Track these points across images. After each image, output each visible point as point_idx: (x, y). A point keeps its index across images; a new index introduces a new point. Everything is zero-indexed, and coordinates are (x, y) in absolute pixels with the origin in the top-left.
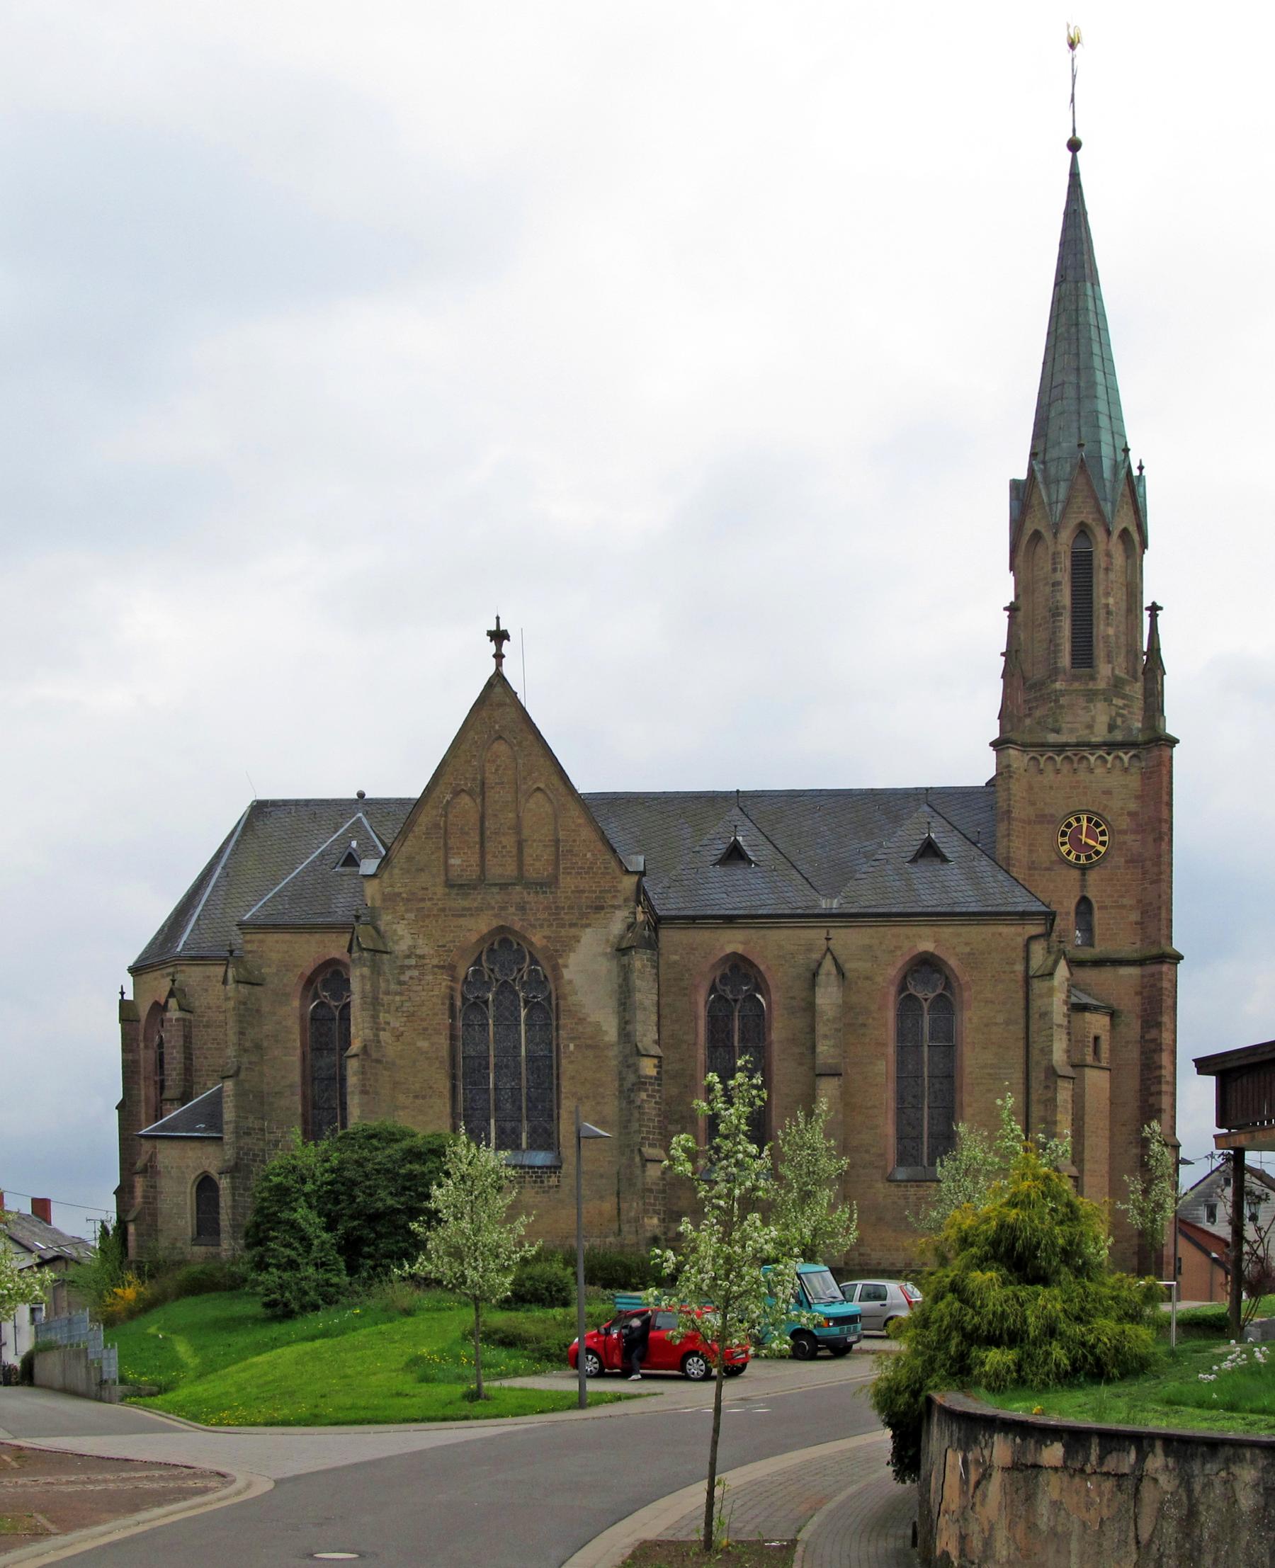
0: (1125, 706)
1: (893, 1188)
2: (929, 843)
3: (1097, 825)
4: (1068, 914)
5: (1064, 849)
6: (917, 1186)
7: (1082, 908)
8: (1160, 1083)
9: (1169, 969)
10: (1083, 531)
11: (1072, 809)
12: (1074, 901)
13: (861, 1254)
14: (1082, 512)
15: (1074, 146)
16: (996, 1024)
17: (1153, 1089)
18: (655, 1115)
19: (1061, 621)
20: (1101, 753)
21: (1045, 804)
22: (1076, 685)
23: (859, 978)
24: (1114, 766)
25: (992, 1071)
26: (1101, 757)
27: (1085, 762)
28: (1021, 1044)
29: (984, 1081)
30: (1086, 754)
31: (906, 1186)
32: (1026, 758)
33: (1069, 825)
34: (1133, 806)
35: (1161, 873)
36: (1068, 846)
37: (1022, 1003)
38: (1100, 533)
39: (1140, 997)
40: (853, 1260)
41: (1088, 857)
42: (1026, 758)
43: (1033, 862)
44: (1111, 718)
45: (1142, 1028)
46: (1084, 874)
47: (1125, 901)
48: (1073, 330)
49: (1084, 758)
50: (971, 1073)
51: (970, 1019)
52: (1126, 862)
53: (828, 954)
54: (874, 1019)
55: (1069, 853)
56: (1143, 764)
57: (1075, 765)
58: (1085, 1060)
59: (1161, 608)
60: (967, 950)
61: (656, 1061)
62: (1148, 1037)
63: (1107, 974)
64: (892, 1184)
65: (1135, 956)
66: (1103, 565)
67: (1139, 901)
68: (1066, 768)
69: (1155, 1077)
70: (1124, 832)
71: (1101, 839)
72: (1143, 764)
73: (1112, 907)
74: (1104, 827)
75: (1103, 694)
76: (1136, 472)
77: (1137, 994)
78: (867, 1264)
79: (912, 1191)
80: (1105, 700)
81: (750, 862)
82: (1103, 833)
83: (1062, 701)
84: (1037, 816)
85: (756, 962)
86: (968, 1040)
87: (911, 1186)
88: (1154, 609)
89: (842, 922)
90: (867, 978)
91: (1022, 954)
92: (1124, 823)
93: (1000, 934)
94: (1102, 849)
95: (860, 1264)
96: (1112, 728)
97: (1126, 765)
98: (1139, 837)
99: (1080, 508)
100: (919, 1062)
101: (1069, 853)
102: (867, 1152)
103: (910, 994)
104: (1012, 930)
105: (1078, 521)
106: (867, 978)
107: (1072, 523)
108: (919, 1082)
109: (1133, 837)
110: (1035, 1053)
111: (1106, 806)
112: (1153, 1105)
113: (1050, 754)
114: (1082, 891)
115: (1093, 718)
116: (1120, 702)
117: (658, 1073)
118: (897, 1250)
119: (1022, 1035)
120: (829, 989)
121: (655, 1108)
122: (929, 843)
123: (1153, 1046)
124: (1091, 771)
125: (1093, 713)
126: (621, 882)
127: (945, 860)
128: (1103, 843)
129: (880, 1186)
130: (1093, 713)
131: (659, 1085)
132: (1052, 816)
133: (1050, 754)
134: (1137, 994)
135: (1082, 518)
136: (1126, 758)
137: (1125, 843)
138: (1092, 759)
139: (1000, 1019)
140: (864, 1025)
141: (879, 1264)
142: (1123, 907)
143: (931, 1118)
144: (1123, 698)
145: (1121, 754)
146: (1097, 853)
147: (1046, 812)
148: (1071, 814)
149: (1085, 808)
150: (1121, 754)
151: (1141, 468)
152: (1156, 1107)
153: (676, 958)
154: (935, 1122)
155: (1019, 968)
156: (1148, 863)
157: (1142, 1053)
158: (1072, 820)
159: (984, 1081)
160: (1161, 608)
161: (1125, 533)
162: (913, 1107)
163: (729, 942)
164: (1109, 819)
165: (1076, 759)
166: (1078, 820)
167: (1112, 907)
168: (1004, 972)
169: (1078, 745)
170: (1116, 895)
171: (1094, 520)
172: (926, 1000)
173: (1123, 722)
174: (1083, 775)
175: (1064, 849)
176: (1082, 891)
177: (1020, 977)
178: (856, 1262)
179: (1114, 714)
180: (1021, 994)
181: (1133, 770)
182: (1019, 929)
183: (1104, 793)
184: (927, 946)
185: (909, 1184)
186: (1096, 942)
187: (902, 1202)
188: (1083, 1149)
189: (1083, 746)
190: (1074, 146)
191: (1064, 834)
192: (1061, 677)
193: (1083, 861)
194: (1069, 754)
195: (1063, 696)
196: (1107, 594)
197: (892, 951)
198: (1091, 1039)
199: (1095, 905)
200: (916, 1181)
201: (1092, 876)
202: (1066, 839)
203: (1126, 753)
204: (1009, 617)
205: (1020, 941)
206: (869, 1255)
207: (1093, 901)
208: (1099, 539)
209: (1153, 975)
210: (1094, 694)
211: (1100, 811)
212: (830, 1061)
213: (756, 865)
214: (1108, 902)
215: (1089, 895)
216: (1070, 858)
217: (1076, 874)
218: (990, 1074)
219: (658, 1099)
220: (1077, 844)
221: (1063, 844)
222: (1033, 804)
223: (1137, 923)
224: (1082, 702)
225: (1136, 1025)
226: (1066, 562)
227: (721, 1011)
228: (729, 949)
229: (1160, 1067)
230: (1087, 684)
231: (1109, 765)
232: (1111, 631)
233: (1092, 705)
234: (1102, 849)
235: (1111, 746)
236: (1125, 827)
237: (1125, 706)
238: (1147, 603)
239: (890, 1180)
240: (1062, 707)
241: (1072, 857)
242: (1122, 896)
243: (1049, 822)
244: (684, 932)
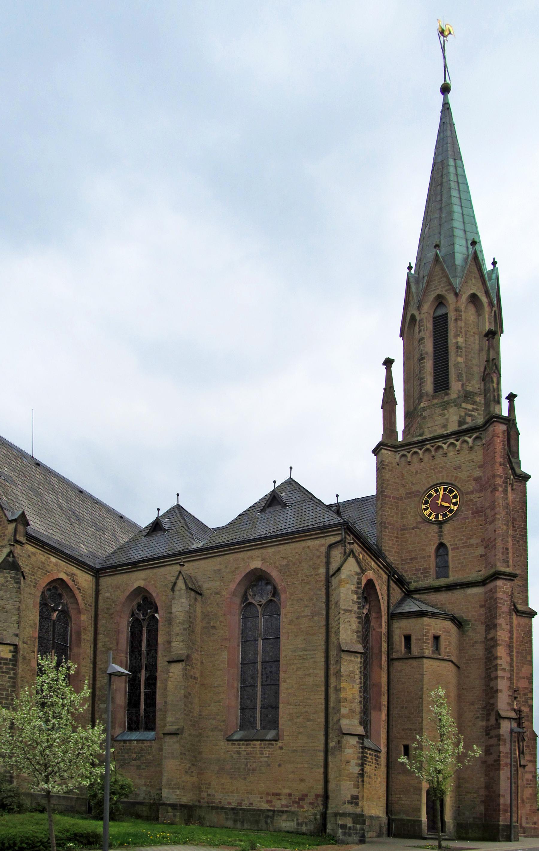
0: (474, 410)
1: (230, 746)
2: (274, 497)
3: (451, 492)
4: (429, 557)
5: (426, 513)
6: (247, 745)
7: (441, 551)
8: (496, 670)
9: (503, 584)
10: (440, 301)
11: (432, 484)
12: (434, 547)
13: (209, 795)
14: (438, 289)
15: (445, 89)
16: (304, 616)
17: (493, 676)
18: (9, 687)
19: (424, 362)
20: (452, 441)
21: (413, 484)
22: (435, 401)
23: (211, 594)
24: (462, 448)
25: (301, 653)
26: (452, 444)
27: (441, 450)
28: (323, 630)
29: (295, 662)
30: (440, 444)
31: (239, 745)
32: (398, 456)
33: (430, 496)
34: (477, 473)
35: (496, 514)
36: (429, 510)
37: (324, 599)
38: (451, 298)
39: (483, 609)
40: (204, 798)
41: (444, 515)
42: (398, 456)
43: (404, 525)
44: (460, 417)
45: (486, 631)
46: (441, 528)
47: (472, 541)
48: (439, 187)
49: (439, 447)
50: (286, 656)
51: (285, 615)
52: (472, 513)
53: (181, 576)
54: (221, 622)
55: (430, 515)
56: (484, 441)
57: (433, 453)
58: (423, 653)
59: (515, 396)
60: (285, 562)
61: (11, 648)
62: (489, 637)
63: (458, 594)
64: (230, 743)
65: (479, 579)
66: (454, 318)
67: (483, 540)
68: (427, 457)
69: (493, 666)
70: (472, 492)
71: (453, 501)
72: (484, 441)
73: (462, 547)
74: (456, 492)
75: (454, 402)
76: (489, 267)
77: (481, 606)
78: (212, 802)
79: (243, 748)
80: (456, 406)
81: (166, 530)
82: (455, 497)
83: (424, 414)
84: (407, 494)
85: (150, 592)
86: (284, 631)
87: (243, 744)
88: (511, 397)
89: (201, 555)
90: (217, 593)
91: (324, 560)
92: (471, 486)
93: (308, 547)
94: (454, 508)
95: (208, 803)
96: (460, 423)
97: (471, 445)
98: (482, 494)
99: (436, 286)
100: (256, 653)
101: (430, 515)
102: (214, 719)
103: (250, 602)
104: (318, 542)
105: (436, 294)
106: (217, 593)
107: (432, 296)
108: (256, 667)
109: (478, 495)
110: (332, 635)
111: (456, 478)
112: (492, 688)
113: (415, 450)
114: (440, 539)
115: (447, 420)
116: (470, 407)
117: (13, 656)
118: (232, 792)
119: (324, 623)
120: (181, 601)
121: (9, 682)
122: (274, 497)
123: (492, 643)
124: (445, 455)
125: (446, 417)
126: (7, 529)
127: (285, 506)
128: (455, 504)
129: (223, 744)
130: (446, 417)
131: (13, 665)
132: (418, 491)
133: (415, 450)
134: (481, 606)
135: (438, 292)
136: (470, 440)
137: (472, 500)
138: (445, 446)
139: (307, 612)
140: (214, 627)
141: (240, 804)
142: (472, 545)
143: (263, 693)
144: (472, 404)
145: (467, 438)
146: (451, 511)
147: (413, 490)
148: (431, 488)
149: (441, 481)
150: (467, 438)
151: (494, 263)
152: (495, 689)
153: (108, 595)
154: (266, 696)
155: (322, 570)
156: (488, 511)
157: (486, 650)
158: (432, 492)
159: (295, 662)
160: (515, 396)
161: (474, 298)
162: (251, 686)
163: (136, 580)
164: (459, 485)
165: (433, 449)
166: (437, 491)
167: (462, 547)
168: (311, 576)
169: (434, 438)
170: (465, 539)
171: (446, 291)
172: (260, 605)
173: (472, 420)
174: (439, 459)
175: (426, 513)
176: (440, 539)
177: (323, 577)
178: (206, 800)
179: (463, 414)
180: (324, 591)
181: (476, 448)
182: (323, 541)
183: (455, 469)
184: (256, 564)
185: (241, 743)
186: (451, 574)
187: (236, 756)
188: (422, 721)
189: (437, 438)
190: (445, 89)
191: (426, 502)
192: (425, 398)
193: (441, 518)
194: (428, 446)
195: (425, 410)
196: (457, 336)
197: (234, 571)
198: (431, 640)
199: (450, 548)
200: (246, 740)
201: (446, 528)
202: (428, 506)
203: (470, 437)
204: (386, 368)
205: (323, 549)
206: (214, 795)
207: (448, 544)
208: (450, 302)
209: (491, 590)
210: (448, 404)
211: (452, 482)
212: (180, 652)
213: (168, 532)
214: (460, 544)
215: (444, 541)
216: (431, 518)
217: (435, 528)
218: (300, 656)
219: (12, 675)
220: (436, 508)
221: (426, 509)
222: (404, 486)
223: (481, 556)
224: (438, 411)
225: (482, 629)
226: (429, 325)
227: (137, 628)
228: (136, 586)
229: (496, 658)
230: (444, 399)
231: (458, 448)
232: (460, 359)
233: (446, 412)
234: (454, 508)
235: (458, 434)
236: (472, 489)
237: (474, 410)
238: (504, 394)
239: (229, 740)
240: (424, 418)
241: (432, 518)
242: (470, 538)
243: (415, 496)
244: (112, 578)
